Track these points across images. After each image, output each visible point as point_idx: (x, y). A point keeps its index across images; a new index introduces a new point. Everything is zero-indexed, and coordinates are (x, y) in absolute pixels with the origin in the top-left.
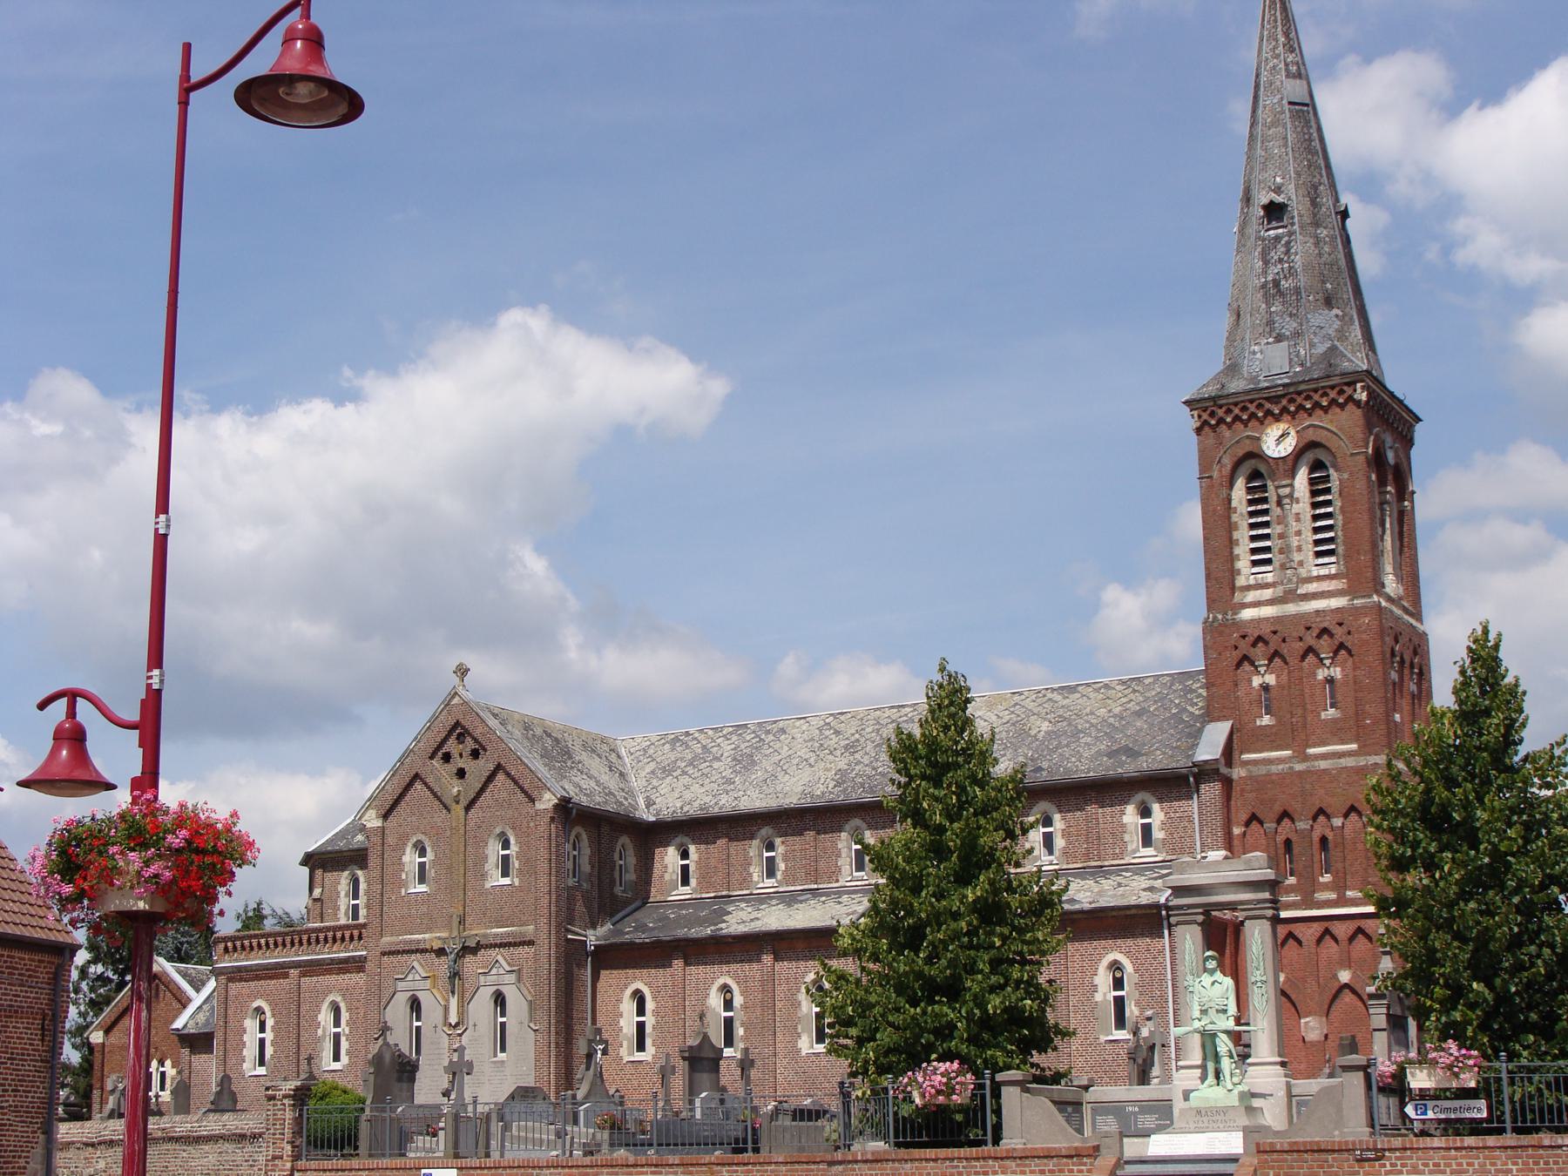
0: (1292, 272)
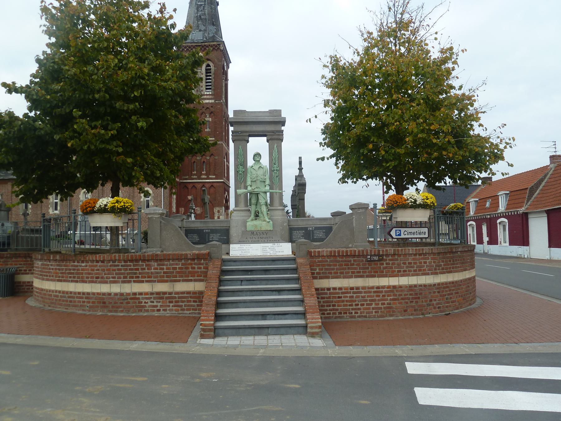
0: (204, 14)
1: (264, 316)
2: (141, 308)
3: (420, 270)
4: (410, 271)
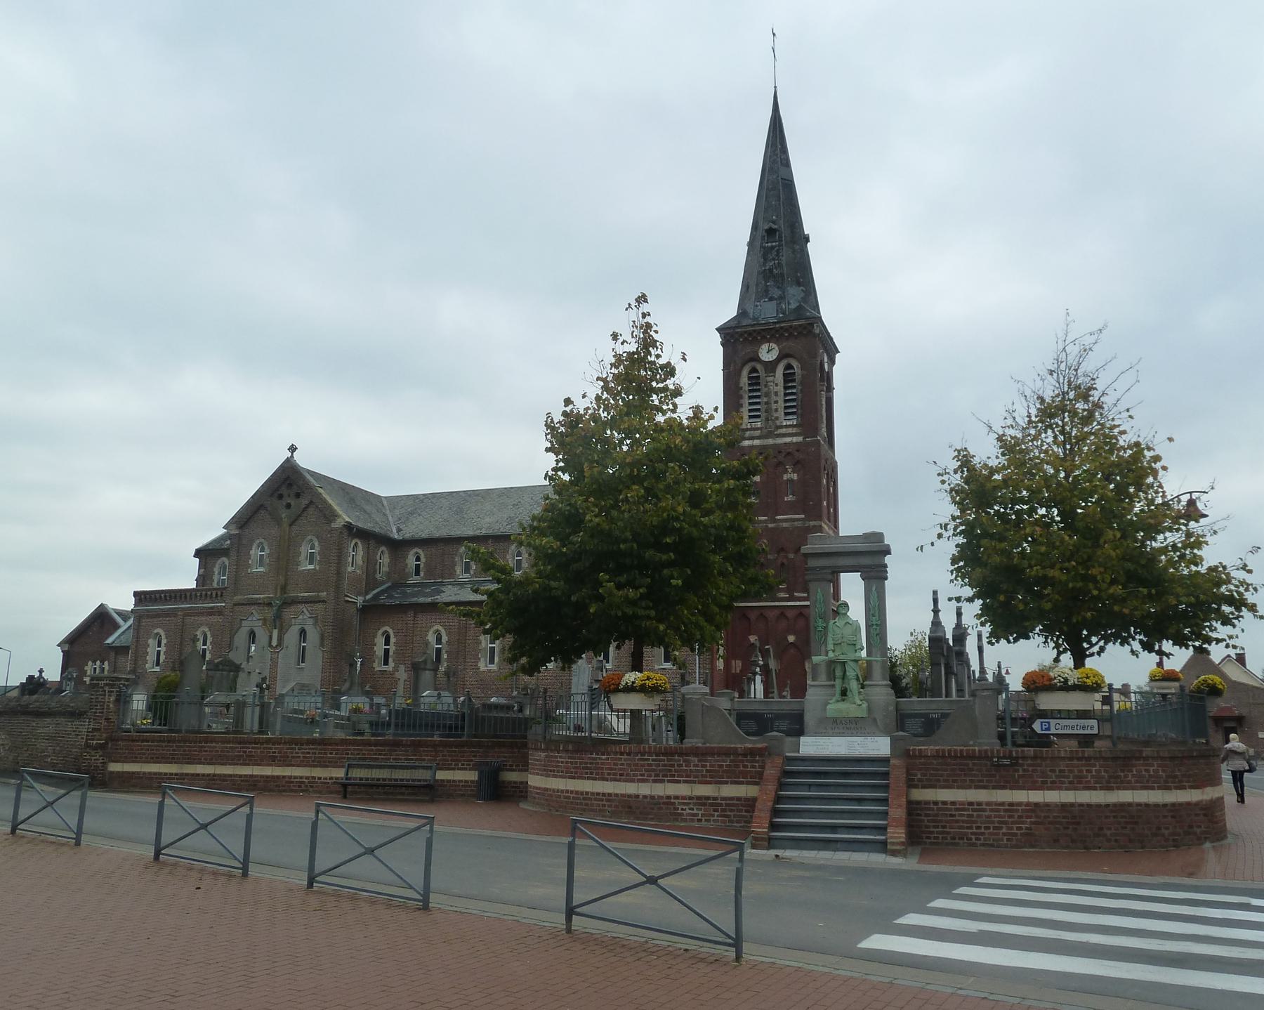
1: (834, 828)
2: (677, 816)
3: (1080, 782)
4: (1063, 783)
